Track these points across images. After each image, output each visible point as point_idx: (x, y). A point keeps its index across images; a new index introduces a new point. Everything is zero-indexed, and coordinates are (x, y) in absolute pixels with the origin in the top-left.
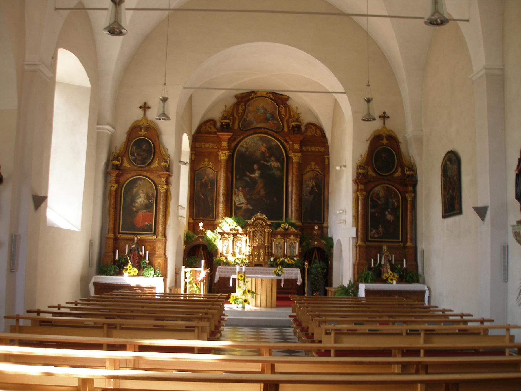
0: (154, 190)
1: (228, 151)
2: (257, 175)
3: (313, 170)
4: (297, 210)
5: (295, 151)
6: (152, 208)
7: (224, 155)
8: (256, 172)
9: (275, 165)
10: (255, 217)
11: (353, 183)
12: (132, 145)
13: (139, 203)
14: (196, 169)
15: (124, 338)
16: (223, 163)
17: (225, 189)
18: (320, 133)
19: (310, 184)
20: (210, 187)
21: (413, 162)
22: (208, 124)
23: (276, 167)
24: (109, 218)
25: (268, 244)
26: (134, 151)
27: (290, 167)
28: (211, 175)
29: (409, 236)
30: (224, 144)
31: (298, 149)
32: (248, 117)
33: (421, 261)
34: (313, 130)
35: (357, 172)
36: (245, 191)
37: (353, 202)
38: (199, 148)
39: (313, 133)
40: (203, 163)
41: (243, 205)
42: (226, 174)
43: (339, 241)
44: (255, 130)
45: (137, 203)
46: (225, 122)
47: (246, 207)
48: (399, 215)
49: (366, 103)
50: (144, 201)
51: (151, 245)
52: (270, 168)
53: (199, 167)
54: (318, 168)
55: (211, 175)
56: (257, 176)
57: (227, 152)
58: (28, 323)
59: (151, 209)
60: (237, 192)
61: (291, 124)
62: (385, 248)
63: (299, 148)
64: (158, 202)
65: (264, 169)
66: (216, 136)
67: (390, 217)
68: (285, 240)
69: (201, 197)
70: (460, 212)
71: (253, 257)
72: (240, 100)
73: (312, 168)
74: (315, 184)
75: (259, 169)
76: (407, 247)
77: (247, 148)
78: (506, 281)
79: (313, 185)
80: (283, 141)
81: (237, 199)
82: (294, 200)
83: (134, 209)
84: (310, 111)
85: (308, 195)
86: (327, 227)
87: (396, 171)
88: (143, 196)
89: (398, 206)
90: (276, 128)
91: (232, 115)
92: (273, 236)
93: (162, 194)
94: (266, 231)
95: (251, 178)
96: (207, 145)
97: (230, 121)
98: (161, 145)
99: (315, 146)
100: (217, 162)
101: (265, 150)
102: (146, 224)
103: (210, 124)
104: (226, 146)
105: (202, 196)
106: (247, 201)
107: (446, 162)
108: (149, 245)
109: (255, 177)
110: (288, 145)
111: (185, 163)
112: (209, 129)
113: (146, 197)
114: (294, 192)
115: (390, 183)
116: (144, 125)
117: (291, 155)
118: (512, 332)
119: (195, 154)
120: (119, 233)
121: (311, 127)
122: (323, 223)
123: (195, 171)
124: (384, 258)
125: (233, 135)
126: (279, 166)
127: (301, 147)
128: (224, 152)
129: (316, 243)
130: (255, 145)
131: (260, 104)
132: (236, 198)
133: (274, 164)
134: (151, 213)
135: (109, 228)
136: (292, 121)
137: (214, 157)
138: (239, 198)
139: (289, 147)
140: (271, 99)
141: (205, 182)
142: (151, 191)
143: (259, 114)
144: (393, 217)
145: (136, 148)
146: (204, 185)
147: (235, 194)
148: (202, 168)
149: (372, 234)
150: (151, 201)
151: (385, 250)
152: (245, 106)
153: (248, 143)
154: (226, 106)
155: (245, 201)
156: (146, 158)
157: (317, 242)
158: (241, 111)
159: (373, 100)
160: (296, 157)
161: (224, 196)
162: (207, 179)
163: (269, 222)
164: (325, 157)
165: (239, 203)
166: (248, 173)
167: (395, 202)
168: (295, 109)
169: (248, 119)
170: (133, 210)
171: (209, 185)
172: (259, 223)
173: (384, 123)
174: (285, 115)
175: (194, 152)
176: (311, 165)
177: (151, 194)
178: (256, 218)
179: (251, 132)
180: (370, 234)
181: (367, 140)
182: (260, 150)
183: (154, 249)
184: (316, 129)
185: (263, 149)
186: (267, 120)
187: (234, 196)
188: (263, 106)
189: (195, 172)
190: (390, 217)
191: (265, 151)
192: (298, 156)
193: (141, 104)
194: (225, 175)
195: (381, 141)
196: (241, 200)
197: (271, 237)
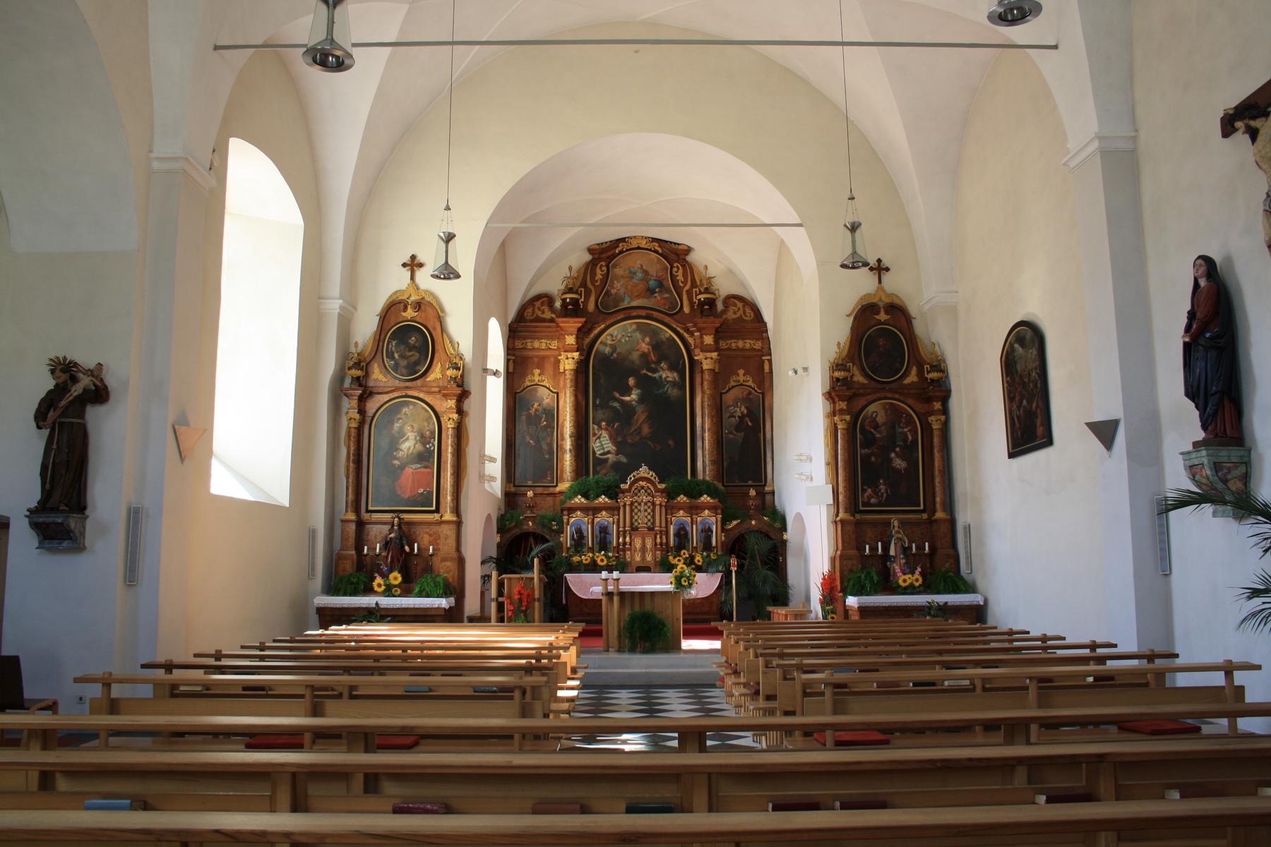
0: (434, 424)
1: (578, 353)
2: (634, 396)
3: (742, 385)
4: (713, 462)
5: (705, 349)
6: (431, 460)
7: (571, 360)
9: (668, 377)
10: (634, 476)
11: (824, 398)
12: (389, 338)
13: (406, 451)
14: (518, 391)
15: (476, 716)
16: (569, 376)
17: (573, 426)
18: (752, 315)
19: (736, 411)
21: (939, 354)
22: (538, 304)
24: (347, 482)
25: (661, 527)
26: (393, 349)
27: (698, 380)
28: (546, 401)
29: (938, 499)
30: (571, 340)
32: (613, 288)
33: (966, 547)
34: (739, 309)
35: (832, 377)
37: (826, 436)
38: (521, 349)
39: (738, 315)
41: (609, 456)
42: (576, 396)
43: (799, 517)
44: (629, 313)
45: (402, 451)
46: (570, 298)
47: (614, 459)
48: (918, 457)
49: (849, 233)
50: (415, 446)
51: (432, 532)
52: (659, 383)
54: (751, 380)
55: (546, 401)
56: (634, 400)
57: (576, 355)
58: (146, 691)
59: (428, 461)
60: (597, 432)
64: (443, 447)
65: (649, 386)
67: (899, 462)
68: (695, 520)
69: (529, 442)
70: (1049, 442)
71: (631, 553)
72: (596, 256)
73: (739, 381)
74: (745, 412)
75: (637, 386)
76: (936, 521)
77: (614, 348)
78: (1166, 572)
79: (742, 413)
80: (682, 331)
82: (707, 442)
83: (396, 462)
84: (731, 272)
85: (734, 432)
86: (773, 493)
87: (905, 375)
88: (413, 437)
89: (915, 441)
90: (667, 307)
91: (584, 285)
92: (669, 512)
93: (450, 431)
94: (658, 502)
95: (622, 402)
98: (445, 336)
99: (743, 339)
100: (557, 373)
101: (649, 349)
102: (421, 491)
103: (543, 304)
105: (531, 441)
106: (616, 447)
107: (1011, 346)
108: (427, 533)
109: (631, 401)
111: (496, 373)
112: (539, 313)
113: (418, 438)
114: (707, 427)
115: (897, 396)
116: (413, 298)
118: (1239, 678)
119: (514, 361)
120: (368, 511)
122: (765, 485)
123: (516, 393)
124: (895, 543)
125: (586, 322)
126: (677, 378)
127: (716, 341)
128: (570, 355)
129: (753, 522)
131: (636, 262)
134: (428, 470)
135: (346, 502)
136: (698, 293)
137: (548, 363)
138: (600, 442)
139: (695, 342)
140: (656, 252)
142: (428, 426)
143: (634, 281)
144: (905, 462)
145: (396, 344)
146: (534, 420)
147: (594, 434)
149: (866, 497)
150: (428, 446)
151: (896, 529)
152: (608, 267)
153: (616, 337)
154: (570, 268)
155: (614, 448)
156: (417, 363)
157: (755, 520)
159: (862, 226)
161: (573, 439)
163: (662, 486)
164: (764, 358)
165: (602, 451)
166: (617, 395)
167: (908, 433)
168: (702, 269)
169: (613, 291)
170: (394, 465)
172: (642, 488)
173: (880, 282)
174: (685, 283)
175: (513, 358)
176: (738, 375)
177: (428, 433)
179: (621, 316)
180: (862, 496)
181: (848, 314)
182: (638, 350)
183: (437, 540)
184: (744, 307)
185: (645, 347)
186: (651, 292)
187: (592, 439)
188: (642, 266)
189: (515, 395)
190: (899, 463)
191: (649, 352)
192: (712, 359)
193: (406, 259)
194: (573, 398)
196: (605, 446)
197: (666, 514)
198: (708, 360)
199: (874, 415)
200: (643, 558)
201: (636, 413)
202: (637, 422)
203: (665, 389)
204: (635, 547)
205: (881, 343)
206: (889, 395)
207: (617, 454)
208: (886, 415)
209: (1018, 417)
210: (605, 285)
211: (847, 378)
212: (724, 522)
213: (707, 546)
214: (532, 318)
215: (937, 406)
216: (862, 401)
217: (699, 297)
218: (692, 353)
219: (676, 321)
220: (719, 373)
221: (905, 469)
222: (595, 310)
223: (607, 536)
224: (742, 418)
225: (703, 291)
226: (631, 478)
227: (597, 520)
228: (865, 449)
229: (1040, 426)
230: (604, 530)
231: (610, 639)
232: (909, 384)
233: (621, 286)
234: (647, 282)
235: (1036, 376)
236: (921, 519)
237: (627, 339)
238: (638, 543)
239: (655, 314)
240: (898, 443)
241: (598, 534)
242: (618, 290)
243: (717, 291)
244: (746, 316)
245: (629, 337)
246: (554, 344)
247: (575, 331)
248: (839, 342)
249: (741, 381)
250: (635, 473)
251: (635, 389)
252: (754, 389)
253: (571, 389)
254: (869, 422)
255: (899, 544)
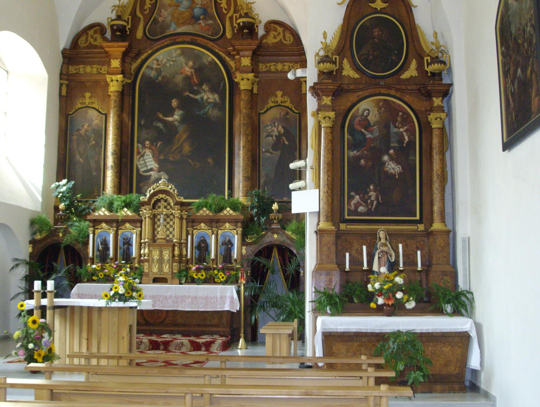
2: (177, 116)
3: (279, 105)
5: (244, 71)
8: (176, 113)
10: (154, 189)
16: (113, 98)
17: (116, 144)
19: (273, 131)
20: (94, 142)
22: (91, 32)
23: (211, 103)
30: (116, 63)
31: (247, 66)
32: (160, 16)
34: (279, 34)
36: (156, 145)
39: (278, 39)
40: (81, 101)
48: (415, 160)
52: (200, 104)
53: (74, 108)
54: (289, 101)
56: (177, 120)
60: (141, 151)
61: (236, 23)
62: (382, 234)
63: (249, 65)
66: (102, 50)
71: (149, 265)
73: (277, 102)
74: (282, 131)
75: (179, 107)
77: (159, 71)
79: (279, 132)
80: (224, 55)
81: (142, 162)
85: (271, 150)
87: (403, 68)
89: (412, 143)
90: (210, 32)
95: (165, 123)
96: (88, 69)
97: (128, 23)
101: (192, 72)
103: (95, 32)
104: (119, 66)
105: (81, 160)
109: (173, 122)
110: (232, 62)
112: (92, 41)
115: (393, 92)
117: (238, 78)
121: (274, 27)
124: (379, 258)
126: (218, 100)
130: (173, 64)
132: (139, 160)
133: (207, 96)
136: (238, 17)
141: (85, 133)
143: (181, 9)
144: (400, 166)
147: (139, 153)
148: (79, 109)
151: (383, 241)
153: (161, 62)
155: (157, 166)
157: (277, 234)
158: (150, 6)
160: (245, 81)
161: (115, 156)
162: (89, 128)
165: (145, 169)
166: (161, 116)
167: (404, 133)
169: (160, 19)
171: (92, 139)
175: (67, 82)
178: (155, 190)
179: (167, 41)
180: (349, 204)
181: (339, 2)
182: (181, 73)
184: (284, 31)
185: (188, 70)
186: (195, 19)
187: (136, 157)
189: (68, 116)
191: (192, 75)
194: (116, 118)
195: (371, 4)
196: (148, 164)
197: (187, 227)
198: (245, 81)
199: (365, 114)
200: (161, 269)
201: (177, 133)
202: (179, 141)
203: (207, 109)
204: (153, 260)
205: (376, 34)
206: (383, 91)
207: (159, 171)
208: (380, 113)
209: (513, 94)
210: (153, 14)
211: (333, 71)
212: (244, 236)
213: (227, 257)
214: (85, 45)
215: (437, 101)
216: (353, 98)
217: (239, 21)
218: (233, 75)
219: (218, 46)
220: (258, 94)
221: (400, 174)
222: (143, 36)
223: (130, 247)
224: (279, 137)
225: (243, 15)
226: (150, 191)
227: (120, 232)
228: (353, 151)
229: (536, 96)
230: (128, 243)
231: (107, 349)
232: (407, 80)
233: (168, 14)
234: (193, 10)
235: (531, 30)
236: (417, 230)
237: (172, 63)
238: (156, 255)
239: (199, 40)
240: (392, 145)
241: (122, 246)
242: (164, 18)
243: (256, 16)
244: (286, 40)
245: (173, 61)
246: (104, 69)
247: (250, 53)
248: (325, 32)
249: (279, 102)
250: (154, 186)
251: (177, 110)
252: (291, 109)
253: (115, 110)
254: (360, 121)
255: (384, 259)
